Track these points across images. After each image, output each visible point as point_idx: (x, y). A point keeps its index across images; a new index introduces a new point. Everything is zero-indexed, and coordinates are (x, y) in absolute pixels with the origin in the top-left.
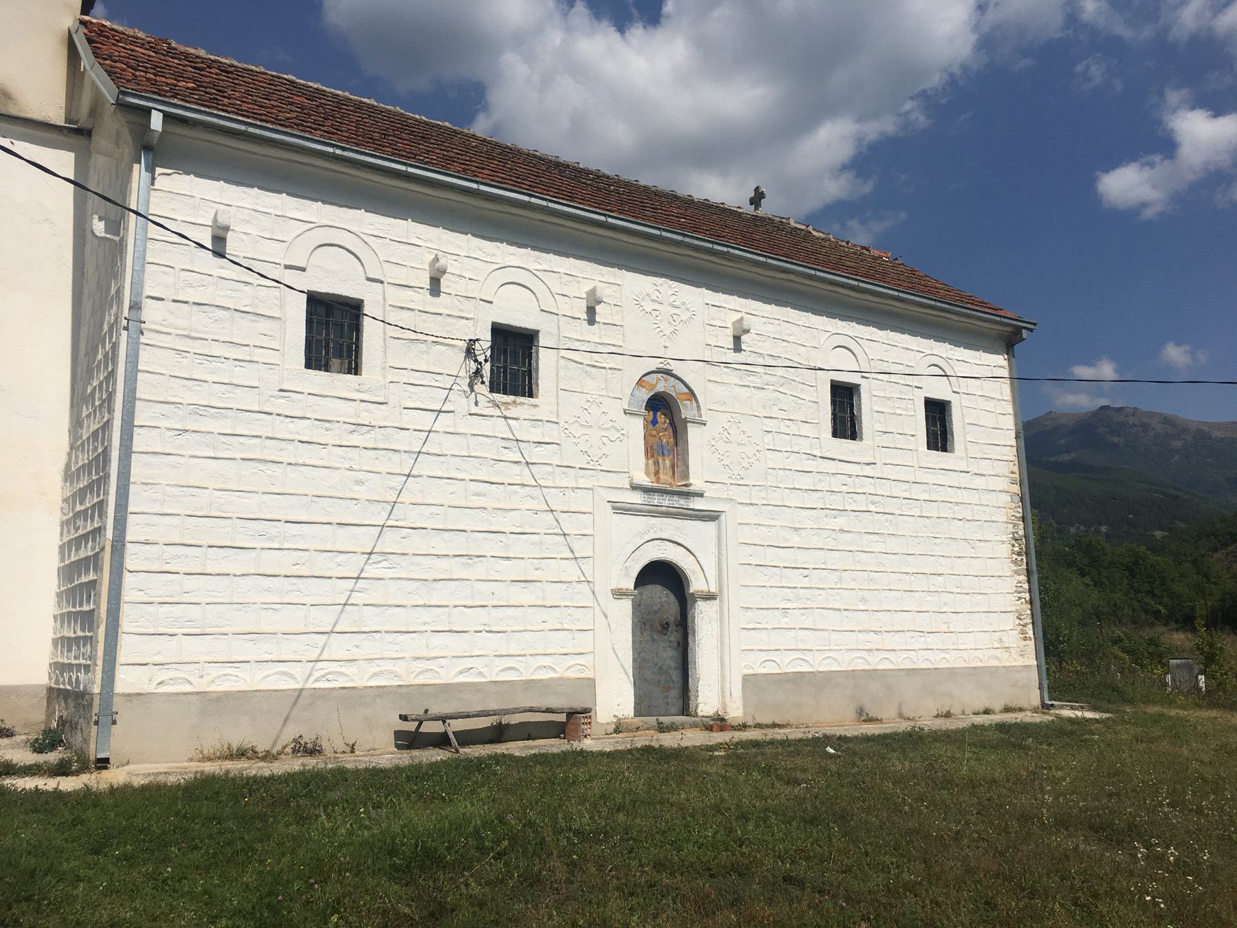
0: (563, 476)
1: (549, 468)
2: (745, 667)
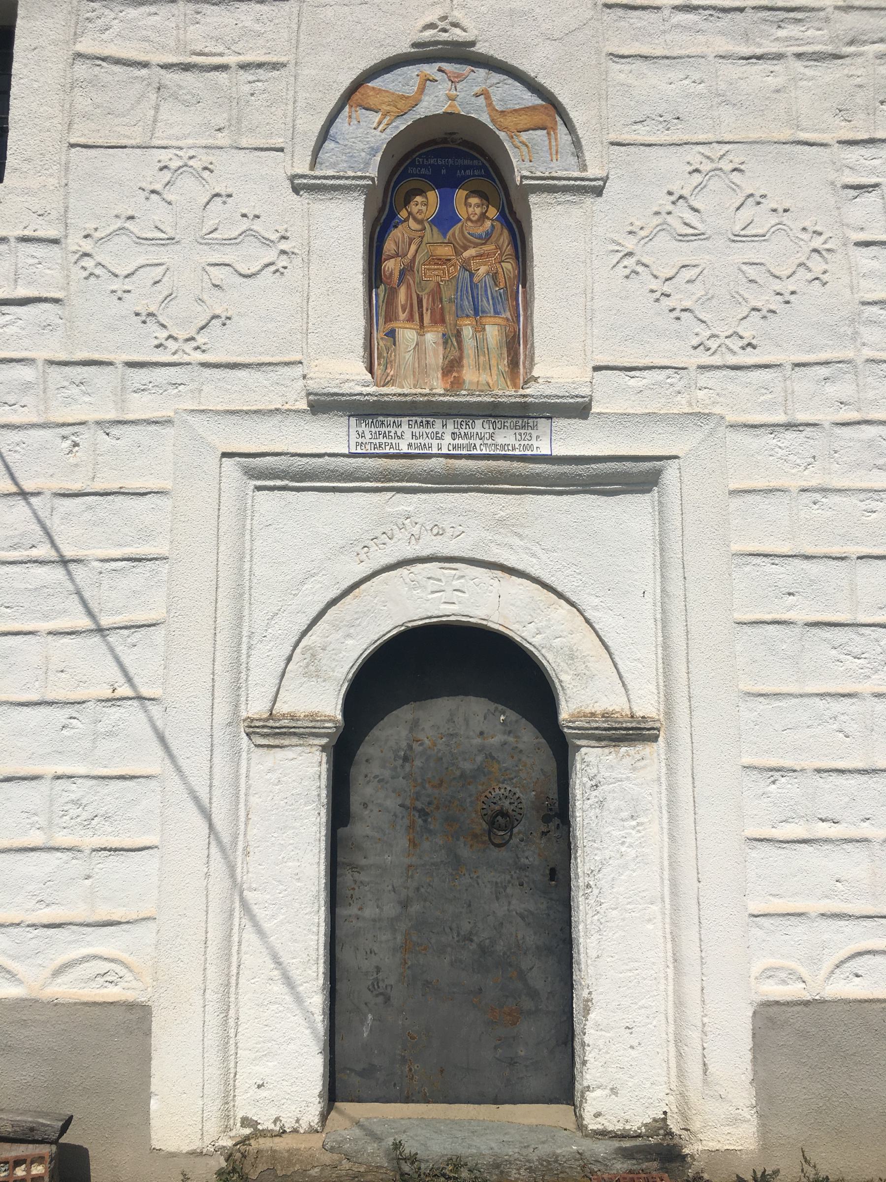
0: (74, 391)
1: (26, 373)
2: (769, 973)
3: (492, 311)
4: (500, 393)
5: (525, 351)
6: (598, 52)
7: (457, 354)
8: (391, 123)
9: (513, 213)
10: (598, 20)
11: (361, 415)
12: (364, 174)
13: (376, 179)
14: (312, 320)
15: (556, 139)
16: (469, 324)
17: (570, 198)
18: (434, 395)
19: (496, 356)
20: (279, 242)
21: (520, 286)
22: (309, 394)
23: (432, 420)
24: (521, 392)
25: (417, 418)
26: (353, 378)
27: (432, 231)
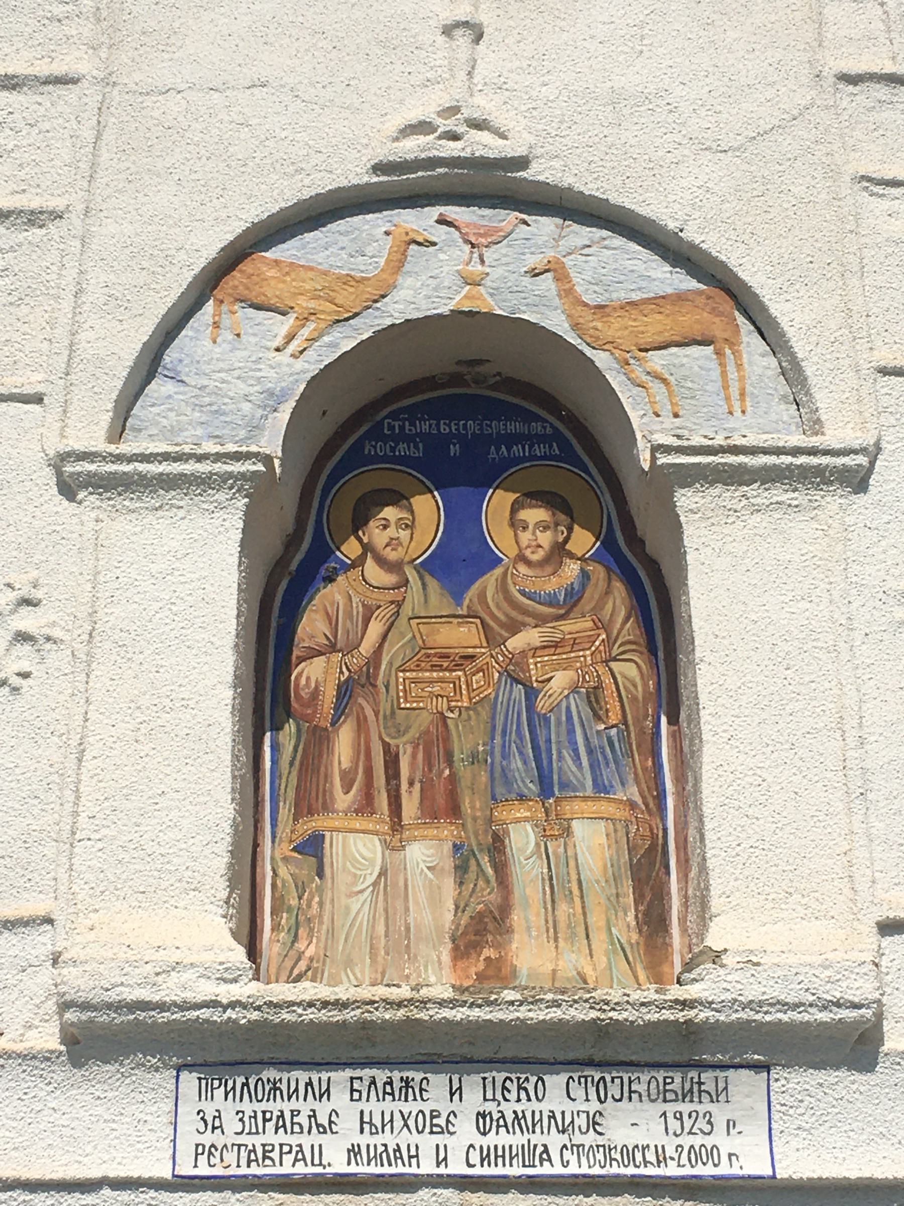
3: (589, 783)
4: (615, 995)
5: (684, 890)
6: (833, 173)
7: (493, 897)
8: (321, 336)
9: (636, 542)
10: (827, 107)
11: (215, 1064)
12: (244, 449)
13: (277, 463)
14: (87, 806)
15: (739, 366)
16: (526, 819)
17: (784, 497)
18: (424, 1003)
19: (603, 900)
20: (13, 612)
21: (664, 719)
22: (65, 1006)
23: (418, 1076)
24: (675, 992)
25: (374, 1072)
26: (194, 959)
27: (424, 585)
